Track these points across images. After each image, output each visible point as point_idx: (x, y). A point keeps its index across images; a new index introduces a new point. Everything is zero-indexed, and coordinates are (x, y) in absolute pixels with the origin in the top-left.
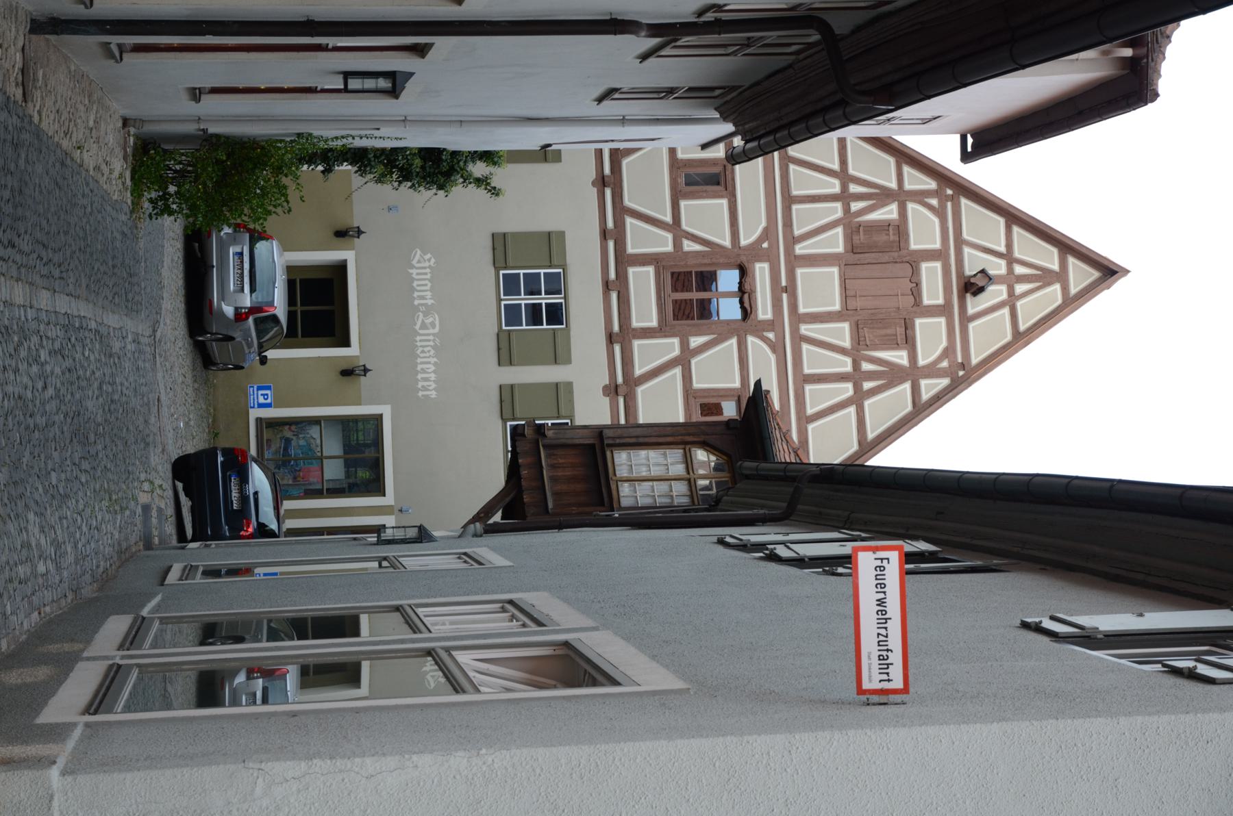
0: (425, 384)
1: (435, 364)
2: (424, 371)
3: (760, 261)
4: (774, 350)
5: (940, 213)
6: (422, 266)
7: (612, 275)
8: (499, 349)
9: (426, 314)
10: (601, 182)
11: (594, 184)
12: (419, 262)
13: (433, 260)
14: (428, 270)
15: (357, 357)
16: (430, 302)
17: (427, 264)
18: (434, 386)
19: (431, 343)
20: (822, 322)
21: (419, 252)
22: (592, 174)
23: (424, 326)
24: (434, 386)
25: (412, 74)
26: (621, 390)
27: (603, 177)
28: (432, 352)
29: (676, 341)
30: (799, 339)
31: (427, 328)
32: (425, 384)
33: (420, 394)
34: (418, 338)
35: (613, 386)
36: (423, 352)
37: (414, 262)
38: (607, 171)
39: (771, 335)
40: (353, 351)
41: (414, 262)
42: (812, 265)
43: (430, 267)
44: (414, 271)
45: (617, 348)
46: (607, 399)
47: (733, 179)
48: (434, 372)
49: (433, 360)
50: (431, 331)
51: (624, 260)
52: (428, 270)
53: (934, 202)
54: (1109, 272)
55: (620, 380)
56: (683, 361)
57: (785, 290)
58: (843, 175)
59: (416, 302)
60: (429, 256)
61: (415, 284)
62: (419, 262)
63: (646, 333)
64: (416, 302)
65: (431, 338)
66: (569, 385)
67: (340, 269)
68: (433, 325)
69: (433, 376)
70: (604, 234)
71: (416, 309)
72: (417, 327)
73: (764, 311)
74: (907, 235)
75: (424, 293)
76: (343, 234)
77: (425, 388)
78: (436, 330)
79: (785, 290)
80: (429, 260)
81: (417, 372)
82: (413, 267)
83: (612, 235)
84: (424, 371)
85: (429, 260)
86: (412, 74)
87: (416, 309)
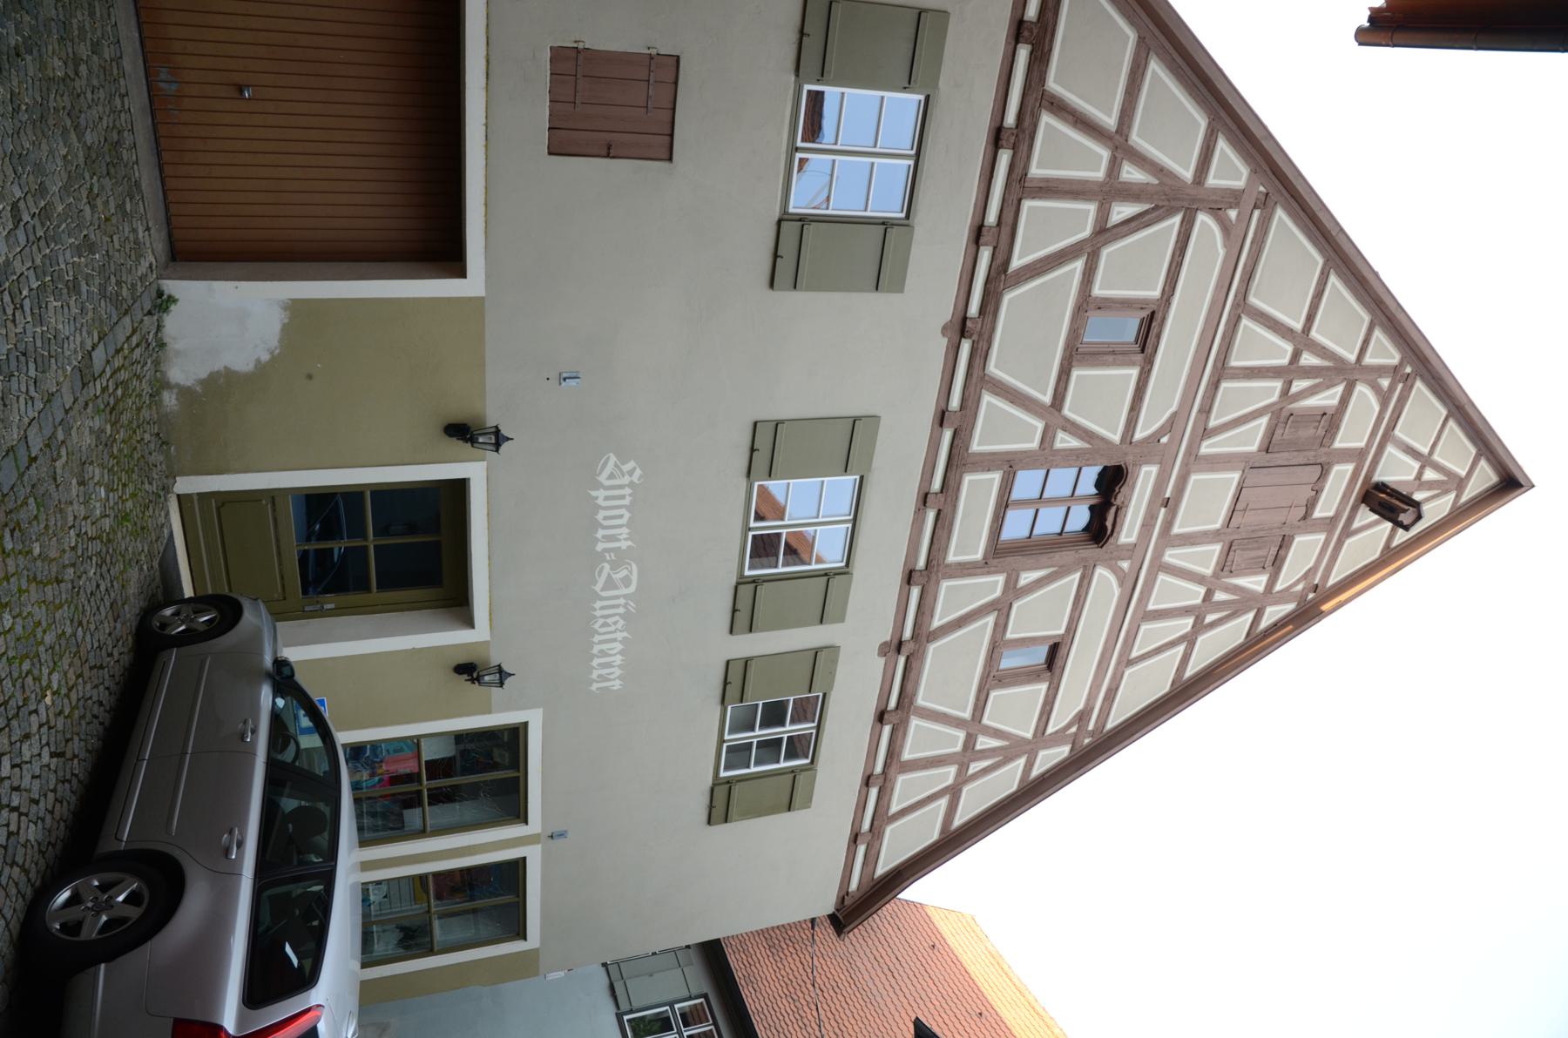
0: (604, 672)
1: (624, 641)
2: (603, 654)
3: (1148, 463)
4: (1121, 584)
5: (1384, 400)
6: (616, 485)
7: (955, 402)
8: (734, 611)
9: (615, 566)
10: (961, 327)
11: (945, 330)
12: (612, 476)
13: (638, 472)
14: (627, 491)
15: (486, 643)
16: (624, 545)
17: (626, 480)
18: (618, 672)
19: (621, 610)
20: (1193, 544)
21: (613, 459)
22: (945, 311)
23: (610, 584)
24: (618, 672)
25: (918, 1023)
26: (905, 650)
27: (965, 319)
28: (622, 622)
29: (1000, 579)
30: (1159, 566)
31: (616, 587)
32: (604, 672)
33: (594, 687)
34: (598, 604)
35: (896, 642)
36: (605, 625)
37: (603, 478)
38: (973, 310)
39: (1125, 565)
40: (478, 634)
41: (603, 478)
42: (1212, 470)
43: (631, 485)
44: (601, 494)
45: (915, 592)
46: (882, 661)
47: (1159, 337)
48: (620, 653)
49: (620, 636)
50: (624, 591)
51: (959, 461)
52: (627, 491)
53: (1385, 383)
54: (605, 965)
55: (907, 634)
56: (1001, 608)
57: (1166, 503)
58: (1302, 340)
59: (600, 547)
60: (632, 464)
61: (601, 515)
62: (612, 476)
63: (966, 569)
64: (600, 547)
65: (622, 601)
66: (833, 650)
67: (459, 488)
68: (626, 581)
69: (618, 659)
70: (942, 418)
71: (600, 557)
72: (598, 588)
73: (1128, 531)
74: (1338, 428)
75: (616, 527)
76: (462, 432)
77: (602, 678)
78: (633, 588)
79: (1166, 503)
80: (631, 473)
81: (592, 657)
82: (598, 486)
83: (953, 420)
84: (603, 654)
85: (631, 473)
86: (918, 1023)
87: (600, 557)
